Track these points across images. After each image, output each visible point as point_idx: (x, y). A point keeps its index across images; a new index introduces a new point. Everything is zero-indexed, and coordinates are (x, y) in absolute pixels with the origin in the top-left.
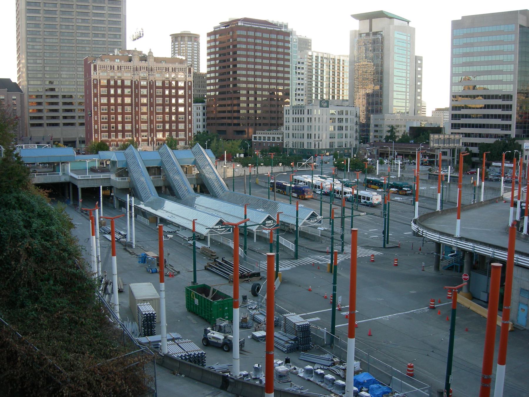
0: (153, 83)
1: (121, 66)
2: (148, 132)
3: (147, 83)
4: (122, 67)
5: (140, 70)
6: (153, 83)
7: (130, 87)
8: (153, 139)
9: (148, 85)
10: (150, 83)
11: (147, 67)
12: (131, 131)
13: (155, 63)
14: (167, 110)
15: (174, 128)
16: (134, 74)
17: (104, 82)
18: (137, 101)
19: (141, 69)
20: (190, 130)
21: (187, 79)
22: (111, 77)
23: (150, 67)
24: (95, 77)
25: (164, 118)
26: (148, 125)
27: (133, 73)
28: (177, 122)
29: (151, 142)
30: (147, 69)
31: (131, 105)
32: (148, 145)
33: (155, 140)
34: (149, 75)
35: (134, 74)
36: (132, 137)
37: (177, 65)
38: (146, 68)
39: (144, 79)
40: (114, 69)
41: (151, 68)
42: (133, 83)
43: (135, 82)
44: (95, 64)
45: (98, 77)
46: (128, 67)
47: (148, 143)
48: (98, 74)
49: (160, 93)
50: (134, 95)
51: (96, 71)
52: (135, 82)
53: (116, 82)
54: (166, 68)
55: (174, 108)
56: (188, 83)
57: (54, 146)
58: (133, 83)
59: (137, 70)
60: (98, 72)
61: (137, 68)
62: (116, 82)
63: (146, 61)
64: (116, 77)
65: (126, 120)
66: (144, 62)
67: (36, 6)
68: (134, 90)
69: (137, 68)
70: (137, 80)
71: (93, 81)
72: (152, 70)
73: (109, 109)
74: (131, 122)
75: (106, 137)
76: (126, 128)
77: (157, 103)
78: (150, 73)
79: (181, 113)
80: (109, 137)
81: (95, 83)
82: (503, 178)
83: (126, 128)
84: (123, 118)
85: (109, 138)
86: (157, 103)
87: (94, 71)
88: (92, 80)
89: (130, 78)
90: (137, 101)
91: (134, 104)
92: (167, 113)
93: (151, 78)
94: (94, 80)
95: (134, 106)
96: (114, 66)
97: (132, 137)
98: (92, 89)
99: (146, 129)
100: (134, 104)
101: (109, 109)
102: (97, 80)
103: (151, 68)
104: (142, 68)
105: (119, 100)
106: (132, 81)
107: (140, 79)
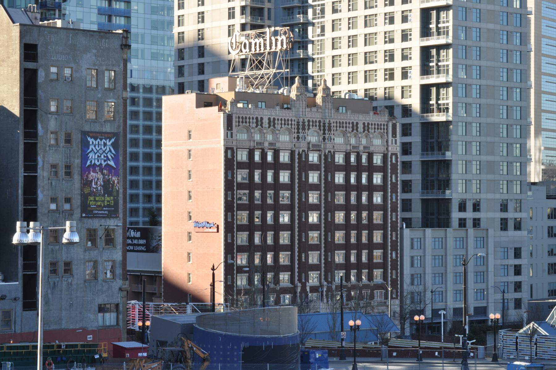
3: (320, 156)
9: (323, 161)
11: (320, 122)
19: (309, 125)
21: (390, 149)
22: (257, 143)
23: (327, 121)
27: (296, 135)
30: (320, 126)
32: (322, 300)
35: (298, 138)
37: (278, 113)
39: (316, 148)
40: (261, 125)
42: (297, 157)
46: (286, 122)
47: (322, 295)
50: (297, 185)
51: (396, 137)
55: (270, 215)
56: (391, 158)
57: (455, 292)
58: (297, 157)
68: (297, 173)
69: (304, 122)
78: (327, 136)
82: (316, 365)
87: (393, 137)
89: (290, 146)
91: (297, 205)
93: (329, 147)
94: (392, 154)
95: (297, 209)
98: (389, 175)
100: (297, 205)
104: (311, 123)
106: (292, 154)
107: (309, 148)
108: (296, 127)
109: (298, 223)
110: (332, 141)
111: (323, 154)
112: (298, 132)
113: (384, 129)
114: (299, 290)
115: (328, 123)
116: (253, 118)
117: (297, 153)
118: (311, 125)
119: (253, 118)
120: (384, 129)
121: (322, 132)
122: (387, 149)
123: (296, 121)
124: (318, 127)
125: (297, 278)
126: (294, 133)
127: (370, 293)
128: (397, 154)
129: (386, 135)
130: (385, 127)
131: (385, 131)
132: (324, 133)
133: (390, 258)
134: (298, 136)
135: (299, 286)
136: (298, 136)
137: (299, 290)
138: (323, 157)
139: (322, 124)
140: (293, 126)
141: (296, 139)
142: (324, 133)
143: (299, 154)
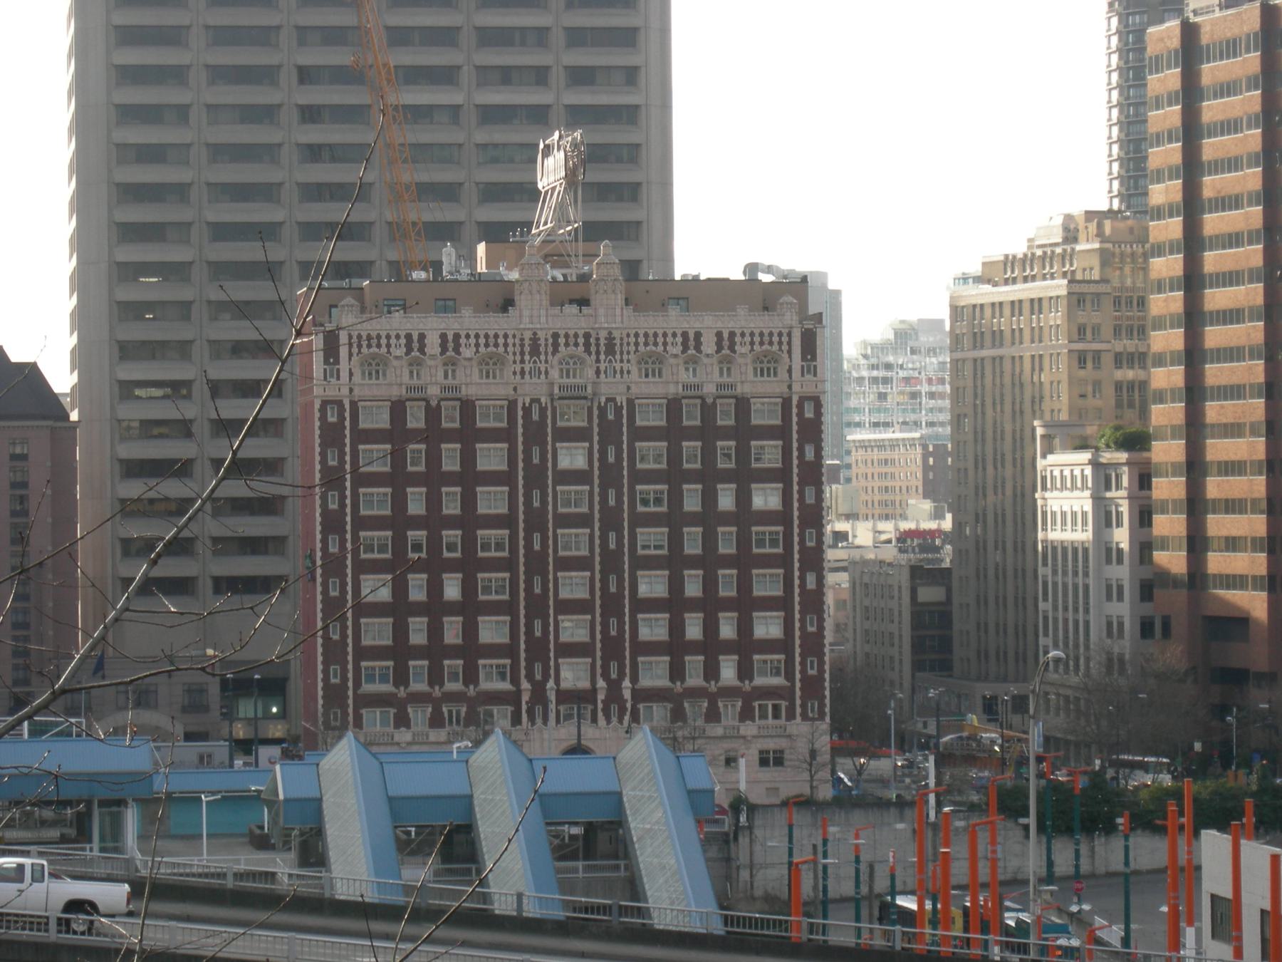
0: (618, 410)
1: (457, 336)
2: (591, 484)
4: (463, 341)
5: (556, 351)
6: (618, 410)
7: (506, 435)
8: (614, 687)
10: (602, 411)
12: (509, 650)
13: (629, 311)
14: (692, 504)
15: (727, 591)
16: (523, 372)
17: (380, 419)
18: (537, 547)
19: (556, 346)
20: (814, 645)
21: (796, 387)
23: (603, 334)
24: (331, 393)
25: (674, 457)
26: (592, 579)
28: (744, 561)
29: (606, 703)
30: (587, 345)
31: (507, 521)
33: (627, 694)
34: (598, 372)
35: (523, 372)
36: (515, 681)
38: (581, 340)
41: (610, 339)
42: (520, 413)
43: (527, 411)
44: (329, 327)
45: (345, 391)
48: (344, 375)
49: (657, 459)
51: (337, 362)
52: (527, 411)
53: (433, 414)
54: (685, 335)
58: (520, 413)
59: (535, 351)
60: (344, 366)
61: (535, 339)
62: (433, 414)
63: (583, 302)
64: (433, 391)
65: (481, 597)
66: (574, 309)
67: (219, 878)
69: (535, 339)
70: (538, 401)
71: (323, 409)
72: (610, 350)
73: (399, 542)
74: (509, 608)
75: (384, 679)
76: (482, 465)
77: (639, 423)
79: (766, 517)
80: (401, 678)
81: (332, 419)
83: (482, 465)
84: (469, 587)
85: (396, 685)
86: (639, 423)
88: (317, 406)
90: (537, 547)
91: (521, 517)
92: (694, 519)
94: (324, 404)
96: (422, 337)
97: (515, 681)
99: (584, 552)
100: (521, 517)
101: (399, 542)
102: (340, 404)
103: (610, 339)
104: (562, 341)
105: (452, 632)
107: (551, 395)
108: (518, 349)
109: (525, 556)
110: (625, 375)
111: (596, 405)
112: (522, 361)
113: (780, 343)
114: (525, 697)
115: (531, 339)
116: (398, 337)
117: (520, 405)
118: (757, 343)
119: (674, 335)
120: (780, 343)
121: (594, 357)
122: (790, 387)
123: (518, 336)
124: (581, 348)
125: (523, 672)
126: (515, 362)
127: (466, 713)
128: (341, 401)
129: (785, 355)
130: (785, 339)
131: (785, 347)
132: (598, 361)
133: (800, 629)
134: (523, 368)
135: (602, 688)
136: (523, 368)
137: (525, 697)
138: (596, 412)
139: (592, 340)
140: (510, 349)
141: (518, 377)
142: (598, 361)
143: (524, 408)
